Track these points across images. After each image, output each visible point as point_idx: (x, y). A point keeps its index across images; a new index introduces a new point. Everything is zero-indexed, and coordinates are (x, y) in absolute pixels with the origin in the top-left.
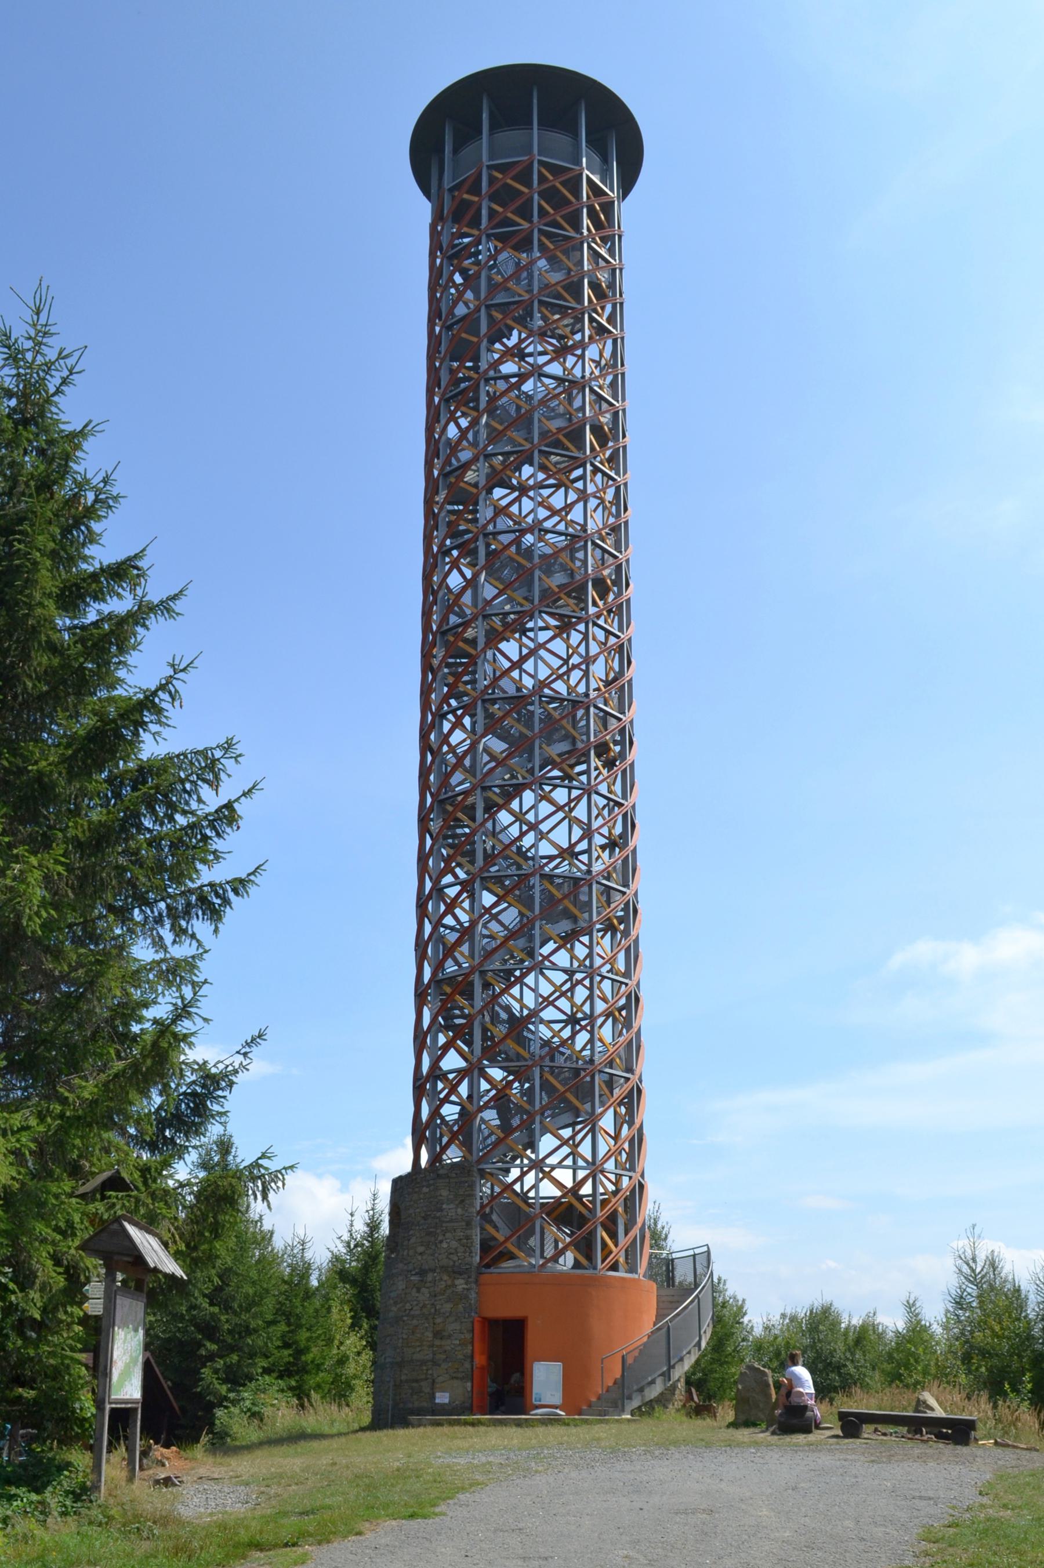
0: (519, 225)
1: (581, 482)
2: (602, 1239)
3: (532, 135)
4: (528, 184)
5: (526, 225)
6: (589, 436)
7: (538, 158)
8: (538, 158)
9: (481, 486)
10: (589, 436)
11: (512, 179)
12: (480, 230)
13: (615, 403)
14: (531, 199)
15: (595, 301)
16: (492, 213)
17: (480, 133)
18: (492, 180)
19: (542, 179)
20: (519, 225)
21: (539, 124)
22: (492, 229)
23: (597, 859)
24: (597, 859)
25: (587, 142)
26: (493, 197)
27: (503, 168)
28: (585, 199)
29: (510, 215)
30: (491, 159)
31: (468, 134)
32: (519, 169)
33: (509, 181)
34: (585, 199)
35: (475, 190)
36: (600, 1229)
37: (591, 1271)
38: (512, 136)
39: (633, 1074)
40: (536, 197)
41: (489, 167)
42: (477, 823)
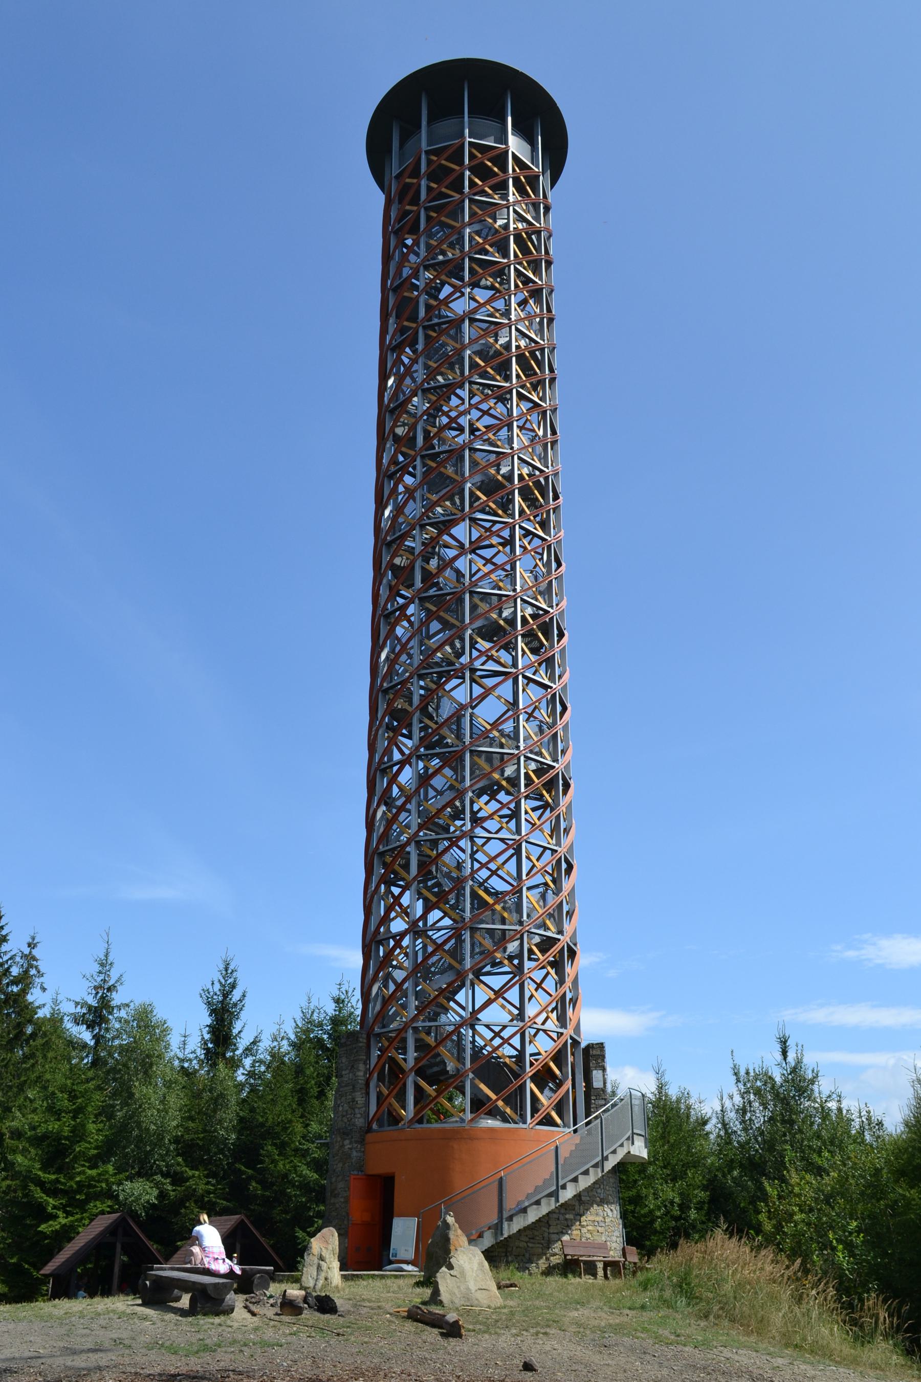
0: (452, 197)
1: (514, 829)
2: (532, 1091)
3: (463, 122)
4: (461, 163)
5: (457, 196)
6: (512, 245)
7: (468, 139)
8: (468, 139)
9: (417, 552)
10: (512, 245)
11: (446, 160)
12: (415, 451)
13: (545, 469)
14: (463, 175)
15: (521, 256)
16: (429, 189)
17: (420, 127)
18: (429, 162)
19: (472, 156)
20: (452, 197)
21: (469, 113)
22: (429, 202)
23: (530, 999)
24: (530, 999)
25: (513, 126)
26: (431, 177)
27: (436, 152)
28: (510, 171)
29: (444, 190)
30: (430, 142)
31: (410, 130)
32: (450, 151)
33: (443, 162)
34: (510, 171)
35: (415, 173)
36: (528, 1081)
37: (521, 1125)
38: (446, 126)
39: (563, 935)
40: (467, 173)
41: (427, 152)
42: (414, 707)
